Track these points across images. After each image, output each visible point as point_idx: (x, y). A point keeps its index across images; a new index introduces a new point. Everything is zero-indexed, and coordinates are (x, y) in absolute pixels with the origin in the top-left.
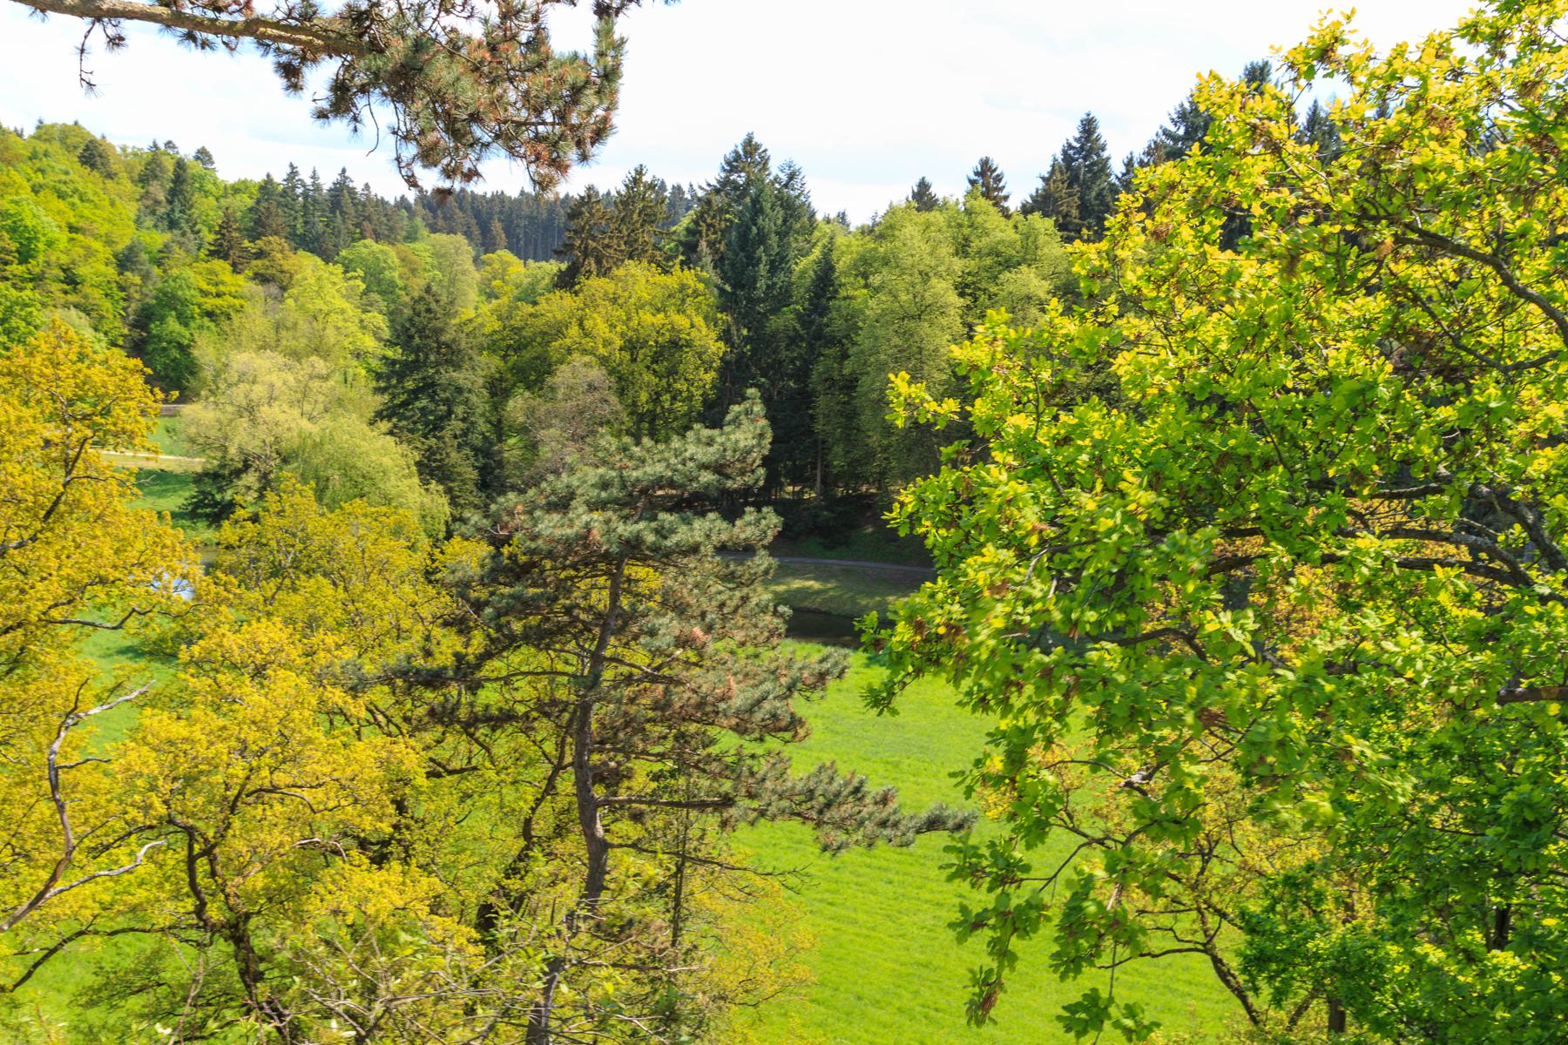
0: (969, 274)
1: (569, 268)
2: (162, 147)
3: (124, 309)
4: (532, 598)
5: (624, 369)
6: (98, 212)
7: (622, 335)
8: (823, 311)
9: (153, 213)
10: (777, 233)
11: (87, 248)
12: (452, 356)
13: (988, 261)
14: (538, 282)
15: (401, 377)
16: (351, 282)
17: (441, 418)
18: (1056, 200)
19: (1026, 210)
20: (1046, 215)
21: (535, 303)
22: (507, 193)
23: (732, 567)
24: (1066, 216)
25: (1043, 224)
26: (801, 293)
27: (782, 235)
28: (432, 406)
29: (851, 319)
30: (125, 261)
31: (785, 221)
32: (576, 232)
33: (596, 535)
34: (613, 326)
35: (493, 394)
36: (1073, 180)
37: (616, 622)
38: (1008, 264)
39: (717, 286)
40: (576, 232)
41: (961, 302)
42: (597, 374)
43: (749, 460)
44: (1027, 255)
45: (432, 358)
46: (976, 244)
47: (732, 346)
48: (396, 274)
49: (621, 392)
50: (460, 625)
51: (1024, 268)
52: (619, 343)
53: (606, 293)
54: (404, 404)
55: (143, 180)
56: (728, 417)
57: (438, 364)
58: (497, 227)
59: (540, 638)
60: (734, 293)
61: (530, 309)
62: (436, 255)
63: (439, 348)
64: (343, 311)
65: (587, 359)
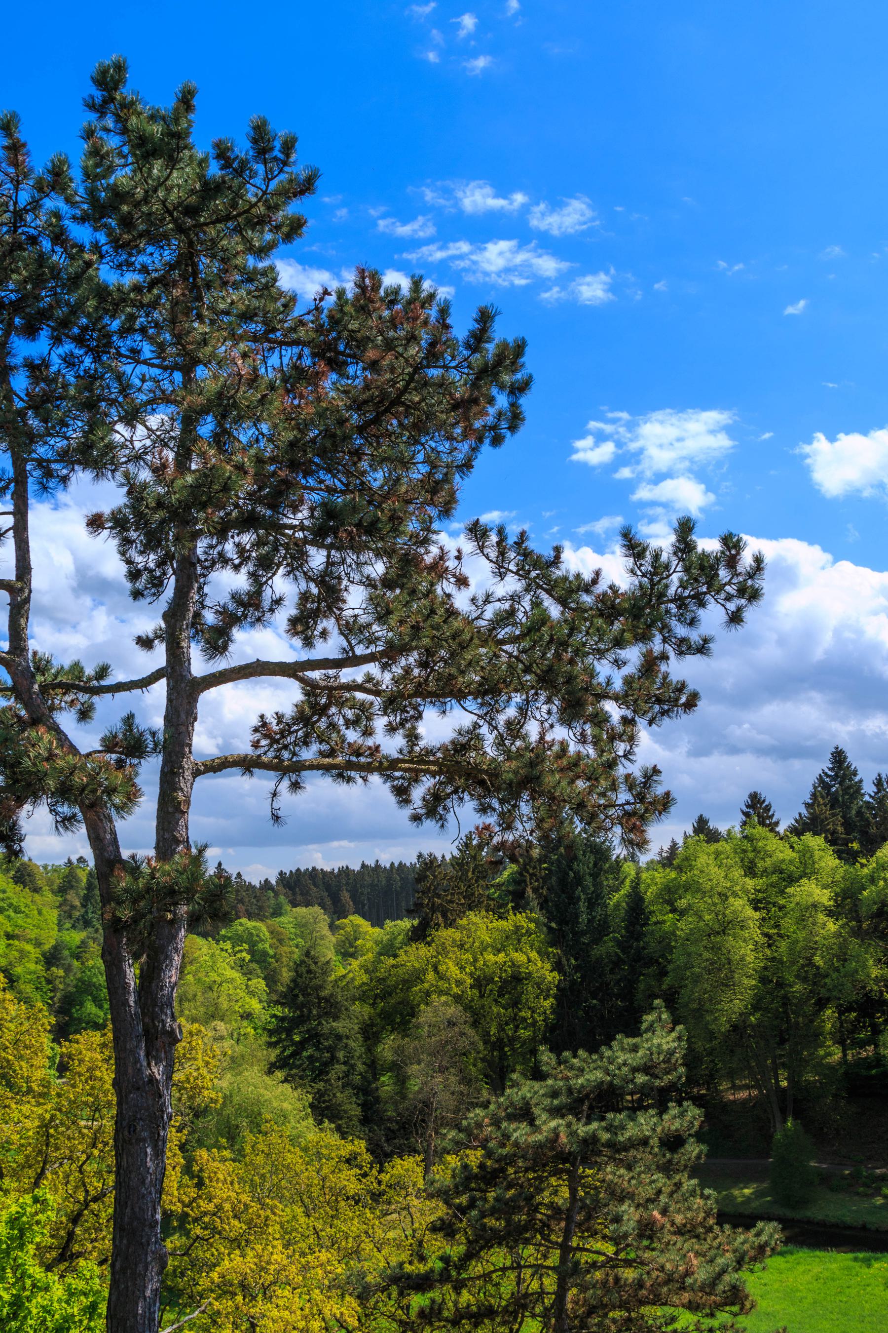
0: (759, 891)
1: (420, 923)
2: (74, 861)
3: (51, 998)
4: (512, 1199)
5: (476, 1003)
6: (29, 920)
7: (471, 975)
8: (639, 936)
9: (70, 917)
10: (591, 875)
11: (21, 951)
12: (332, 1008)
13: (774, 878)
14: (395, 938)
15: (289, 1032)
16: (238, 955)
17: (325, 1064)
18: (822, 821)
19: (798, 830)
20: (816, 833)
21: (395, 956)
22: (351, 867)
23: (668, 1156)
24: (833, 833)
25: (815, 842)
26: (619, 923)
27: (595, 876)
28: (317, 1054)
29: (666, 942)
30: (51, 958)
31: (595, 864)
32: (423, 893)
33: (563, 1139)
34: (462, 968)
35: (366, 1039)
36: (834, 803)
37: (582, 1215)
38: (792, 880)
39: (545, 925)
40: (423, 893)
41: (757, 915)
42: (453, 1011)
43: (673, 1061)
44: (807, 869)
45: (315, 1012)
46: (760, 864)
47: (565, 975)
48: (267, 946)
49: (475, 1024)
50: (445, 1228)
51: (804, 881)
52: (469, 981)
53: (454, 941)
54: (293, 1055)
55: (62, 890)
56: (644, 1026)
57: (319, 1017)
58: (345, 896)
59: (513, 1237)
60: (560, 930)
61: (392, 961)
62: (298, 925)
63: (320, 1003)
64: (232, 980)
65: (443, 998)
